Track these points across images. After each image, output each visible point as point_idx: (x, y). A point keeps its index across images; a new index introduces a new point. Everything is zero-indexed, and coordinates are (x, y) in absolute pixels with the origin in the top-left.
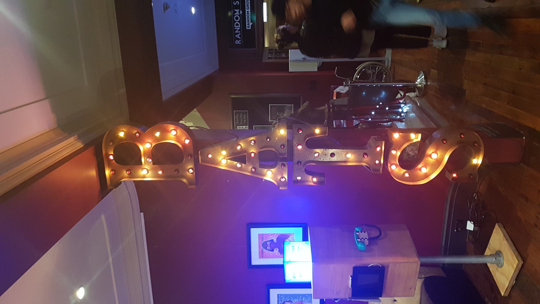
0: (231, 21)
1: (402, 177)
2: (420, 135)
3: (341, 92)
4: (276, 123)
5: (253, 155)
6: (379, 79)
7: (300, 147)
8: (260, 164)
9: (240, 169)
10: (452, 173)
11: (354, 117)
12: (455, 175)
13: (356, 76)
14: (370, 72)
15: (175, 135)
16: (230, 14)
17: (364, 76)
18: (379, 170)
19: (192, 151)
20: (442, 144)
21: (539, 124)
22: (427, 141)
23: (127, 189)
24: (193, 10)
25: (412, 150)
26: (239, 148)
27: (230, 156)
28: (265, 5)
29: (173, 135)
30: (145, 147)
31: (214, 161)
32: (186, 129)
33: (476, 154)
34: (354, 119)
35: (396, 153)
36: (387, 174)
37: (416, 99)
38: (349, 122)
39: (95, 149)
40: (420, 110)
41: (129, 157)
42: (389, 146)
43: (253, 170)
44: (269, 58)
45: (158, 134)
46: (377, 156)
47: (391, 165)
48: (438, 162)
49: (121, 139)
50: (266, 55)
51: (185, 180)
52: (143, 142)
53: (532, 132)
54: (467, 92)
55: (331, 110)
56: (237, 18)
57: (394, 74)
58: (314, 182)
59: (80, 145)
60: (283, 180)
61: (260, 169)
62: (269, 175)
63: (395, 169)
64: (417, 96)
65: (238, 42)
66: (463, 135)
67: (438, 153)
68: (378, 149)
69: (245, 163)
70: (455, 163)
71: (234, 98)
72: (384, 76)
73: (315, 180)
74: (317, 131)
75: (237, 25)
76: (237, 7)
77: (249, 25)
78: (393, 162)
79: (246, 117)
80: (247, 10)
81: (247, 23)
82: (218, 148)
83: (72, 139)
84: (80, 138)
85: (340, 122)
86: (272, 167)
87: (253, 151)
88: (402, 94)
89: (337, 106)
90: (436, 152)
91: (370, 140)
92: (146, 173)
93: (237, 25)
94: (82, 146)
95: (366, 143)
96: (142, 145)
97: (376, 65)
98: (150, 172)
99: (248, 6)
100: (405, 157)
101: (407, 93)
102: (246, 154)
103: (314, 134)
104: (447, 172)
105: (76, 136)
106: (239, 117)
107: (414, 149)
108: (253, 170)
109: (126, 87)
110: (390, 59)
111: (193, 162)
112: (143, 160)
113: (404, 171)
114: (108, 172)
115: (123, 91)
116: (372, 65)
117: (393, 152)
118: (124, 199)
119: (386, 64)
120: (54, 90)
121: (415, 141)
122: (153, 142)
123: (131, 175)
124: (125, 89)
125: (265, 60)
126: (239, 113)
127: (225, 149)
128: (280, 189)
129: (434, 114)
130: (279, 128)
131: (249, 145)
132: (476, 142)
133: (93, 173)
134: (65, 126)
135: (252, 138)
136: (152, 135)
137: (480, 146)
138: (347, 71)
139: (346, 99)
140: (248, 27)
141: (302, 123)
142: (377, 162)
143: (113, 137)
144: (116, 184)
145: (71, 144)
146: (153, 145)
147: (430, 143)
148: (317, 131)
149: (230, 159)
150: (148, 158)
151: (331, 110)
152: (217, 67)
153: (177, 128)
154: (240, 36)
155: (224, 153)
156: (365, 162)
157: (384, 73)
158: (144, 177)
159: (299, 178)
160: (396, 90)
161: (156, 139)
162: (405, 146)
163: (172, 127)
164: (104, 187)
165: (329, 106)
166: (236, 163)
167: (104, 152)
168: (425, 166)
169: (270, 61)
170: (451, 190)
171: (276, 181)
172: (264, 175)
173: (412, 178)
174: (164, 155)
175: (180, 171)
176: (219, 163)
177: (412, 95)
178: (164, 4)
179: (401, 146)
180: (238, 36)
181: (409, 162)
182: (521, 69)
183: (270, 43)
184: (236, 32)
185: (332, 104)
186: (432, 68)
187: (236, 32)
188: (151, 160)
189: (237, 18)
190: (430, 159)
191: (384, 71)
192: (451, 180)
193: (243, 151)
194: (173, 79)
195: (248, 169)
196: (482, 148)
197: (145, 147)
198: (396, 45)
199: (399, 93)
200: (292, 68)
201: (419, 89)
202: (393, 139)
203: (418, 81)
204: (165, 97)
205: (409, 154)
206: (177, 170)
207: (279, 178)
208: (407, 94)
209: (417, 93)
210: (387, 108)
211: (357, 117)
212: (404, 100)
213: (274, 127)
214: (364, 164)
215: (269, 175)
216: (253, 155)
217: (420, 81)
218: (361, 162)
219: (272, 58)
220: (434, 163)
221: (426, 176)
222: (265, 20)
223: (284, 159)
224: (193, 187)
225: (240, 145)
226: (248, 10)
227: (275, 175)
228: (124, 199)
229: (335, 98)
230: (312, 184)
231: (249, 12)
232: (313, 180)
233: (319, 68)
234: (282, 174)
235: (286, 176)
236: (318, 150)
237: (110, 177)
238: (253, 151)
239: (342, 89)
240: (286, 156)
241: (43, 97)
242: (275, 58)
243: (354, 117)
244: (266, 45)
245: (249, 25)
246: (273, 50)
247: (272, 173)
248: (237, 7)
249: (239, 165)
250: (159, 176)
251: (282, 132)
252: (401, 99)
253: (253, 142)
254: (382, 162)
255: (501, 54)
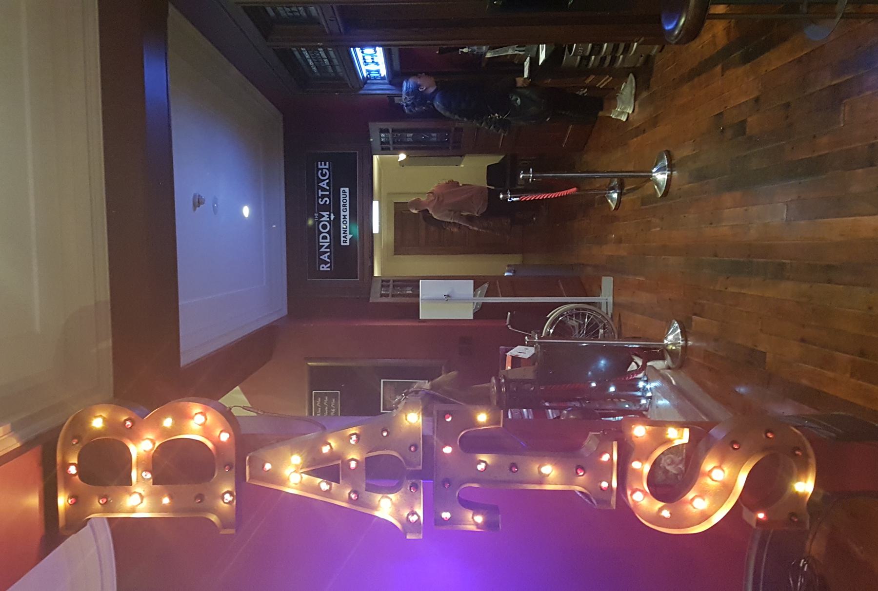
0: (314, 232)
1: (658, 519)
2: (686, 432)
3: (521, 356)
4: (399, 402)
5: (353, 465)
7: (448, 450)
8: (367, 485)
9: (327, 493)
11: (547, 404)
12: (761, 516)
13: (548, 329)
14: (573, 322)
15: (203, 425)
16: (310, 222)
17: (561, 330)
18: (608, 502)
19: (232, 456)
20: (731, 448)
22: (702, 445)
23: (96, 540)
24: (246, 211)
25: (672, 463)
26: (325, 449)
27: (307, 467)
28: (376, 204)
29: (199, 424)
30: (141, 448)
31: (275, 477)
33: (803, 470)
34: (548, 408)
36: (626, 513)
37: (668, 373)
38: (539, 412)
41: (107, 467)
42: (627, 453)
43: (353, 496)
44: (382, 295)
45: (168, 422)
46: (603, 471)
48: (727, 488)
51: (214, 518)
54: (769, 358)
55: (504, 389)
57: (620, 326)
58: (477, 524)
60: (413, 518)
61: (366, 494)
62: (386, 507)
63: (641, 500)
64: (669, 368)
65: (324, 268)
66: (772, 433)
67: (725, 469)
68: (605, 458)
69: (338, 482)
70: (763, 488)
72: (601, 331)
73: (479, 519)
74: (482, 417)
75: (325, 238)
76: (325, 208)
77: (346, 239)
78: (635, 486)
79: (336, 405)
80: (342, 213)
81: (342, 235)
84: (14, 429)
85: (522, 414)
86: (392, 490)
87: (354, 456)
88: (640, 364)
89: (512, 381)
91: (587, 440)
92: (139, 501)
94: (18, 445)
95: (580, 446)
96: (135, 444)
97: (584, 309)
98: (145, 501)
99: (344, 206)
100: (660, 477)
101: (649, 361)
102: (340, 462)
103: (473, 423)
105: (8, 426)
106: (322, 403)
107: (677, 459)
108: (353, 496)
110: (610, 300)
112: (134, 474)
115: (107, 344)
116: (577, 309)
117: (636, 465)
119: (604, 309)
121: (677, 443)
123: (107, 507)
124: (110, 341)
126: (322, 396)
128: (408, 537)
129: (708, 402)
130: (406, 409)
131: (347, 444)
133: (33, 501)
135: (353, 430)
136: (158, 421)
137: (806, 455)
140: (345, 242)
141: (454, 403)
142: (604, 485)
146: (157, 444)
147: (707, 450)
148: (482, 417)
149: (307, 473)
150: (146, 470)
151: (504, 389)
152: (285, 312)
153: (206, 410)
155: (296, 459)
156: (580, 484)
157: (601, 325)
158: (133, 510)
159: (446, 515)
163: (196, 408)
165: (498, 381)
166: (319, 480)
167: (59, 459)
168: (701, 495)
171: (400, 521)
172: (375, 508)
173: (678, 520)
175: (206, 497)
176: (284, 482)
177: (659, 364)
178: (195, 196)
179: (652, 452)
180: (325, 257)
181: (669, 487)
182: (870, 308)
183: (382, 270)
185: (505, 377)
186: (695, 314)
187: (323, 250)
188: (149, 476)
189: (324, 227)
190: (709, 481)
191: (601, 322)
193: (334, 455)
194: (205, 323)
195: (342, 495)
196: (812, 461)
197: (141, 448)
199: (632, 360)
201: (672, 353)
202: (634, 439)
203: (670, 337)
205: (666, 472)
206: (201, 497)
207: (406, 514)
208: (649, 364)
209: (668, 361)
211: (554, 405)
212: (645, 375)
213: (396, 408)
214: (578, 488)
215: (386, 507)
216: (353, 465)
217: (673, 338)
218: (571, 484)
220: (717, 490)
222: (376, 230)
224: (231, 531)
225: (329, 444)
226: (345, 213)
227: (397, 508)
229: (509, 368)
230: (472, 528)
231: (348, 217)
232: (474, 520)
233: (475, 314)
234: (412, 507)
235: (420, 511)
236: (484, 457)
238: (355, 457)
242: (393, 296)
243: (547, 404)
244: (376, 274)
245: (346, 239)
246: (389, 281)
247: (393, 504)
248: (325, 208)
249: (324, 486)
250: (164, 509)
251: (413, 419)
252: (638, 372)
253: (354, 437)
254: (615, 484)
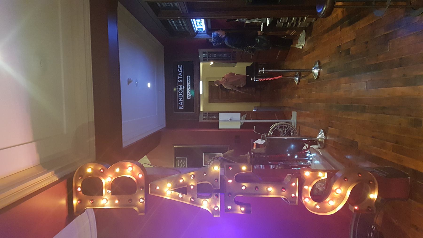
0: (176, 94)
1: (315, 209)
3: (260, 143)
4: (211, 162)
5: (192, 187)
6: (288, 133)
7: (230, 181)
8: (198, 195)
10: (354, 205)
11: (270, 163)
12: (356, 208)
13: (270, 132)
14: (281, 130)
15: (132, 171)
17: (276, 132)
18: (295, 202)
19: (143, 183)
20: (344, 180)
21: (422, 167)
23: (89, 217)
24: (149, 85)
25: (320, 186)
26: (181, 181)
28: (201, 82)
29: (130, 171)
30: (107, 180)
31: (160, 192)
32: (141, 167)
33: (373, 189)
34: (271, 164)
35: (308, 188)
36: (302, 206)
37: (319, 150)
38: (267, 166)
39: (67, 183)
40: (323, 158)
41: (93, 188)
43: (192, 200)
45: (118, 170)
46: (293, 190)
47: (305, 198)
48: (342, 197)
49: (90, 174)
50: (201, 116)
51: (136, 209)
52: (105, 176)
53: (416, 173)
55: (253, 157)
56: (180, 91)
57: (300, 131)
58: (242, 211)
59: (56, 179)
62: (205, 204)
63: (308, 201)
64: (319, 148)
65: (180, 108)
66: (361, 174)
67: (342, 189)
68: (294, 184)
69: (186, 194)
70: (357, 196)
71: (177, 148)
72: (292, 133)
73: (243, 209)
74: (244, 168)
75: (181, 96)
77: (189, 96)
78: (306, 196)
80: (188, 86)
82: (164, 181)
83: (50, 174)
84: (56, 173)
85: (260, 167)
87: (193, 184)
88: (308, 146)
89: (256, 153)
90: (339, 188)
92: (106, 202)
93: (181, 96)
94: (57, 179)
98: (108, 202)
99: (189, 83)
100: (315, 192)
102: (187, 186)
103: (240, 170)
104: (350, 205)
105: (53, 172)
106: (179, 162)
107: (323, 185)
108: (192, 200)
109: (96, 135)
110: (296, 121)
111: (144, 193)
113: (316, 203)
114: (75, 202)
115: (94, 138)
116: (282, 125)
117: (306, 187)
118: (86, 223)
119: (293, 124)
120: (42, 134)
121: (322, 178)
122: (114, 176)
123: (93, 204)
125: (201, 120)
126: (180, 160)
127: (170, 182)
128: (214, 216)
129: (335, 162)
130: (213, 165)
131: (189, 179)
132: (371, 181)
133: (64, 202)
134: (45, 164)
135: (192, 173)
136: (113, 170)
137: (374, 184)
138: (263, 128)
139: (264, 148)
140: (189, 97)
142: (293, 195)
143: (82, 170)
144: (81, 210)
145: (50, 177)
146: (113, 179)
148: (244, 168)
150: (109, 189)
151: (253, 157)
152: (165, 126)
153: (133, 165)
154: (182, 104)
155: (169, 185)
156: (283, 195)
157: (292, 131)
159: (229, 207)
160: (302, 143)
161: (117, 174)
162: (315, 182)
163: (129, 164)
164: (71, 214)
166: (178, 193)
167: (74, 185)
168: (332, 199)
169: (205, 121)
170: (354, 221)
171: (211, 210)
172: (201, 205)
173: (323, 209)
174: (122, 187)
176: (164, 194)
177: (315, 147)
178: (128, 79)
181: (319, 196)
182: (400, 124)
183: (204, 109)
184: (180, 100)
185: (253, 152)
186: (330, 127)
187: (180, 100)
188: (110, 192)
190: (335, 194)
191: (292, 130)
192: (353, 211)
193: (184, 183)
194: (133, 130)
195: (188, 199)
196: (377, 186)
197: (107, 180)
198: (331, 30)
199: (304, 145)
200: (221, 126)
201: (320, 142)
204: (124, 145)
205: (318, 190)
206: (131, 200)
207: (213, 207)
208: (311, 146)
209: (319, 146)
210: (296, 157)
213: (210, 164)
214: (282, 197)
215: (205, 204)
216: (192, 187)
217: (321, 136)
218: (280, 195)
219: (206, 119)
220: (338, 198)
221: (334, 208)
222: (201, 92)
223: (217, 191)
224: (143, 214)
227: (210, 205)
228: (86, 223)
230: (240, 213)
232: (241, 210)
233: (241, 126)
234: (216, 204)
235: (219, 206)
236: (244, 184)
237: (77, 206)
239: (261, 142)
240: (219, 188)
241: (31, 140)
242: (208, 119)
243: (270, 163)
244: (201, 110)
246: (206, 113)
247: (208, 203)
249: (181, 196)
250: (116, 205)
251: (216, 169)
252: (306, 150)
253: (192, 176)
254: (297, 195)
255: (384, 113)
